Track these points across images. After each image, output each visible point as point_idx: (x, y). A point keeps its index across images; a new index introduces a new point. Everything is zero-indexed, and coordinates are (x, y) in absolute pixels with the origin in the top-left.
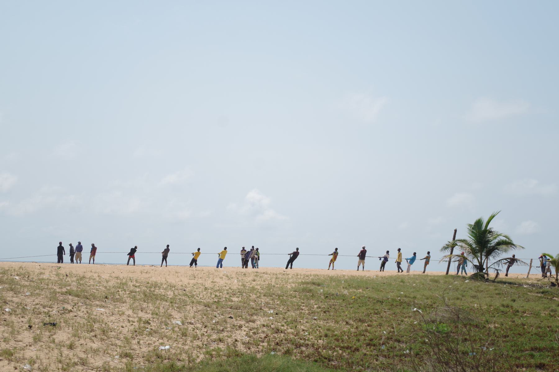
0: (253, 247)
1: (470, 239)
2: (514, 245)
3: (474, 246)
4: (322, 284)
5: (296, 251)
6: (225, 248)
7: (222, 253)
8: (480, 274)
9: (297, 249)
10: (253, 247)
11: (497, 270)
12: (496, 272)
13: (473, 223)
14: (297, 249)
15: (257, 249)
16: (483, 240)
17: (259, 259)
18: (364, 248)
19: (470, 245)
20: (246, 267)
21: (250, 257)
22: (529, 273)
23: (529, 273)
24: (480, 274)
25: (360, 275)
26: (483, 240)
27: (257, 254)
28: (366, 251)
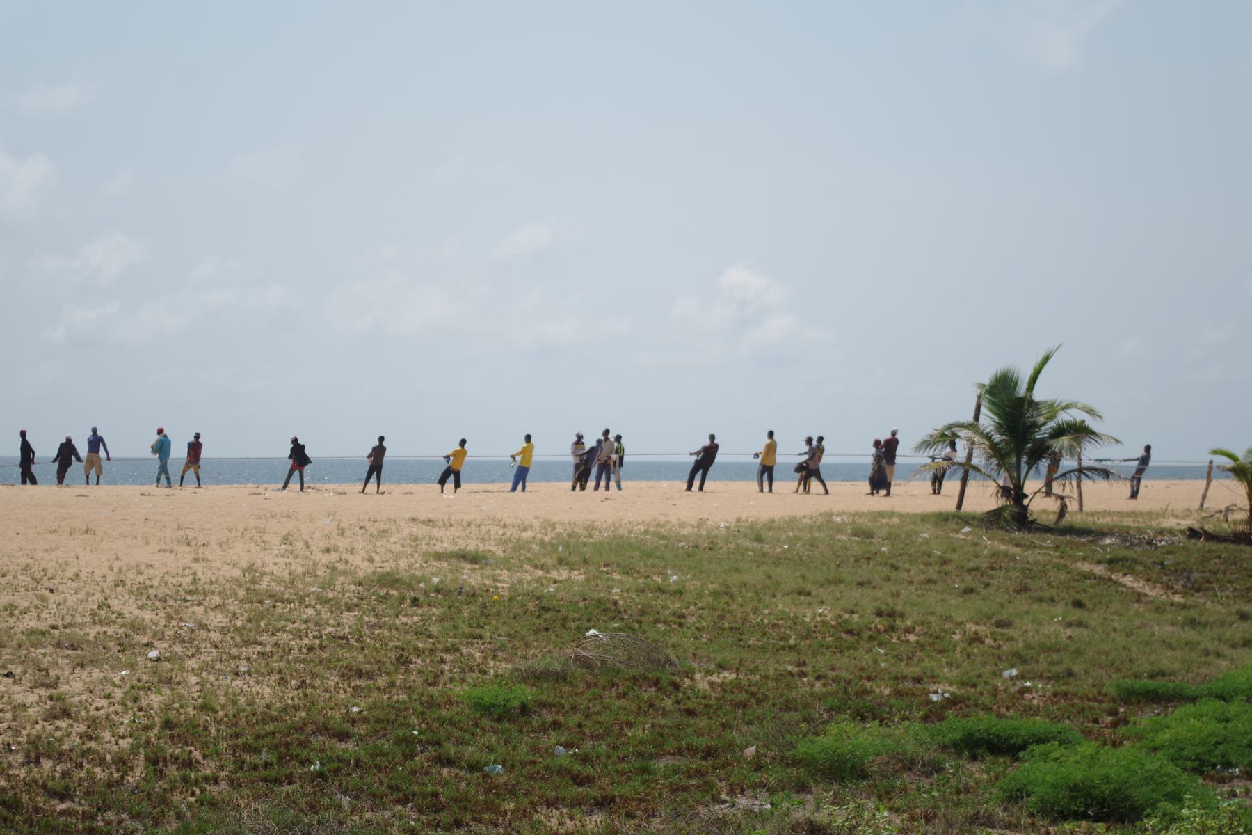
0: (607, 432)
1: (988, 421)
2: (1094, 433)
3: (997, 438)
4: (485, 558)
5: (707, 443)
6: (528, 438)
7: (454, 455)
8: (1014, 515)
9: (712, 437)
10: (607, 432)
11: (1062, 498)
12: (1059, 502)
13: (987, 380)
14: (712, 437)
15: (618, 438)
16: (1020, 427)
17: (621, 464)
18: (894, 434)
19: (988, 437)
20: (583, 488)
21: (596, 463)
22: (1204, 497)
23: (1204, 497)
24: (1014, 515)
25: (225, 563)
26: (1020, 427)
27: (620, 452)
28: (897, 441)
